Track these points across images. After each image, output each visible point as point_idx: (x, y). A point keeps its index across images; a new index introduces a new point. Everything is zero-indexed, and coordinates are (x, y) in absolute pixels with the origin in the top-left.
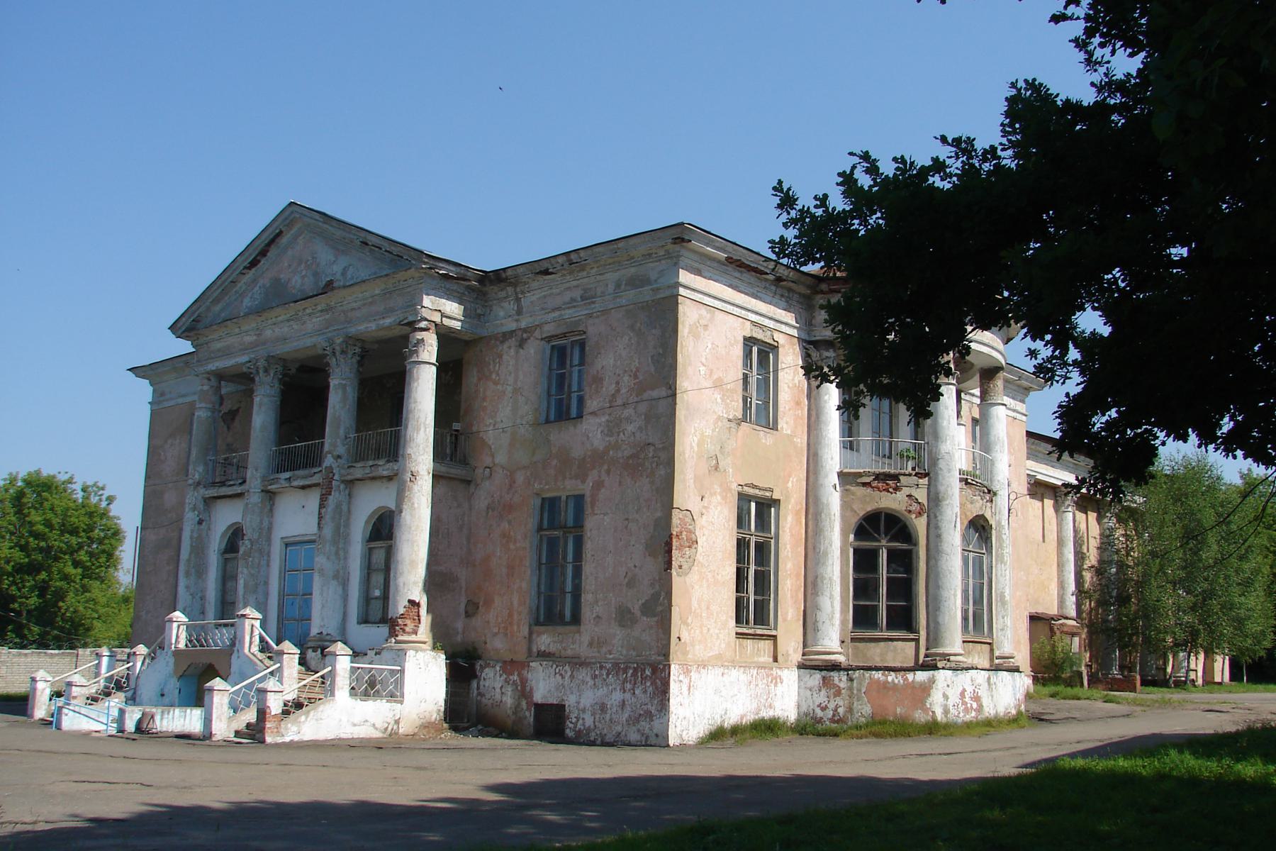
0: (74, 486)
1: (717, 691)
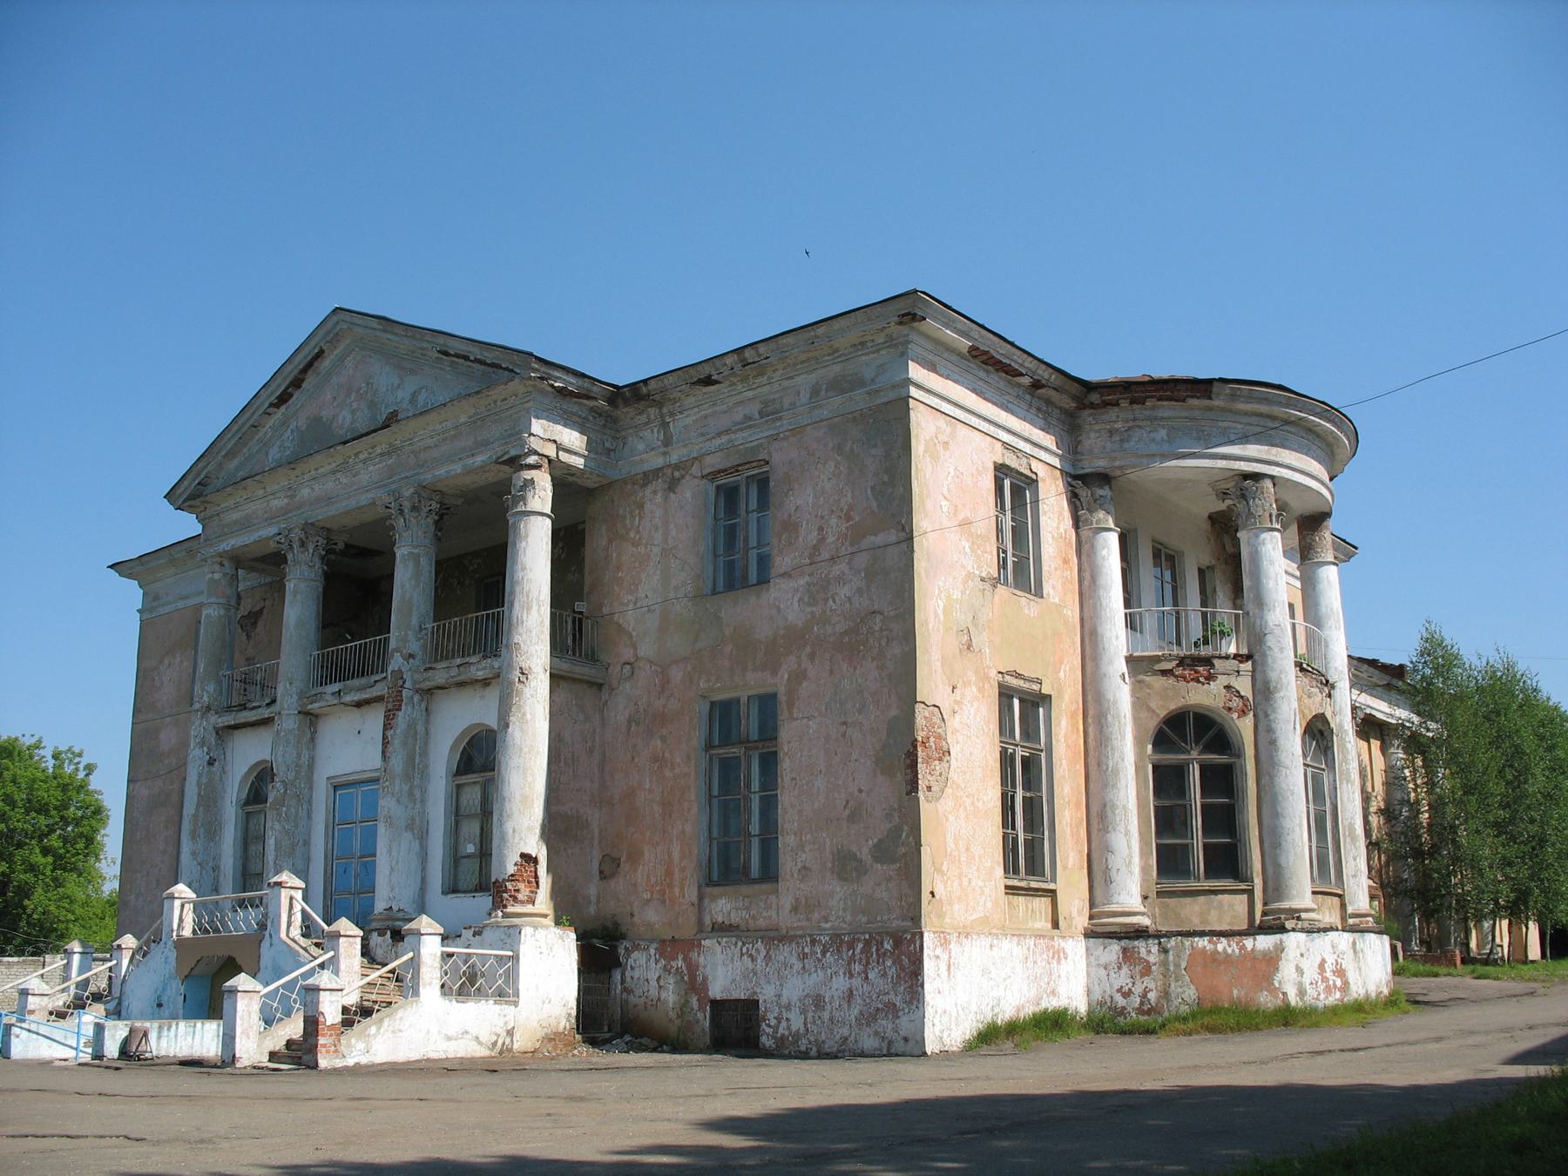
0: (42, 752)
1: (985, 972)
